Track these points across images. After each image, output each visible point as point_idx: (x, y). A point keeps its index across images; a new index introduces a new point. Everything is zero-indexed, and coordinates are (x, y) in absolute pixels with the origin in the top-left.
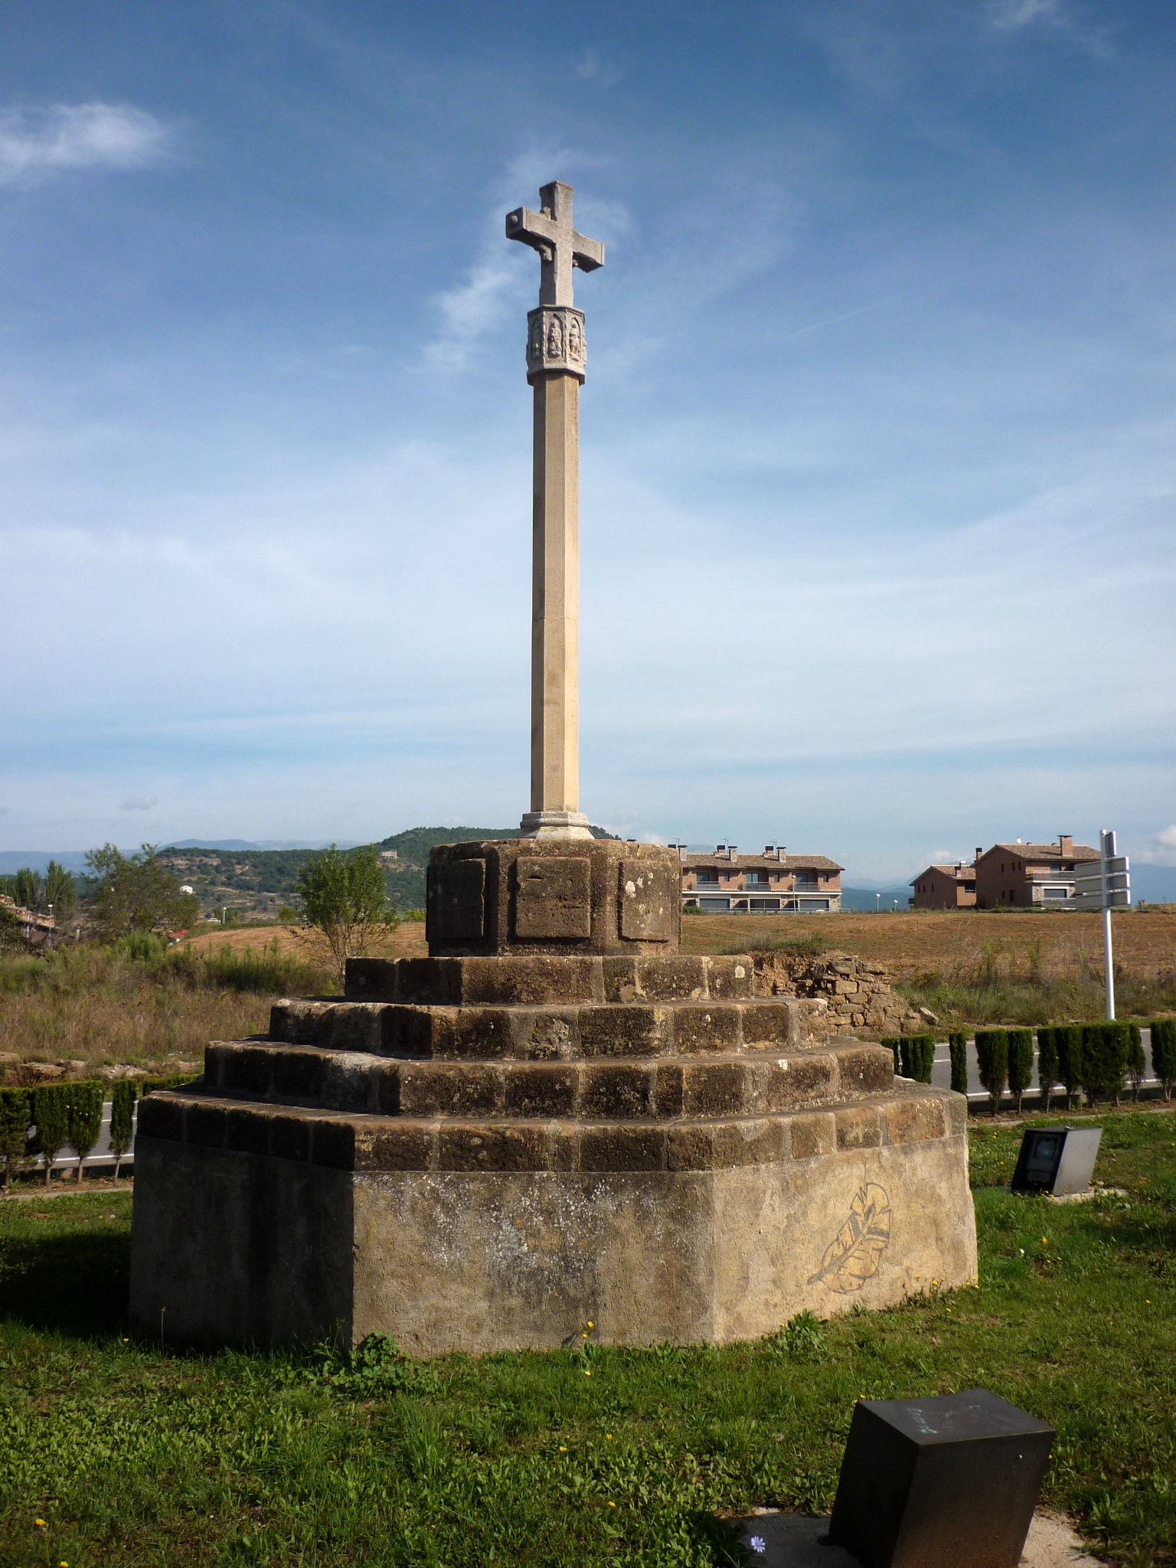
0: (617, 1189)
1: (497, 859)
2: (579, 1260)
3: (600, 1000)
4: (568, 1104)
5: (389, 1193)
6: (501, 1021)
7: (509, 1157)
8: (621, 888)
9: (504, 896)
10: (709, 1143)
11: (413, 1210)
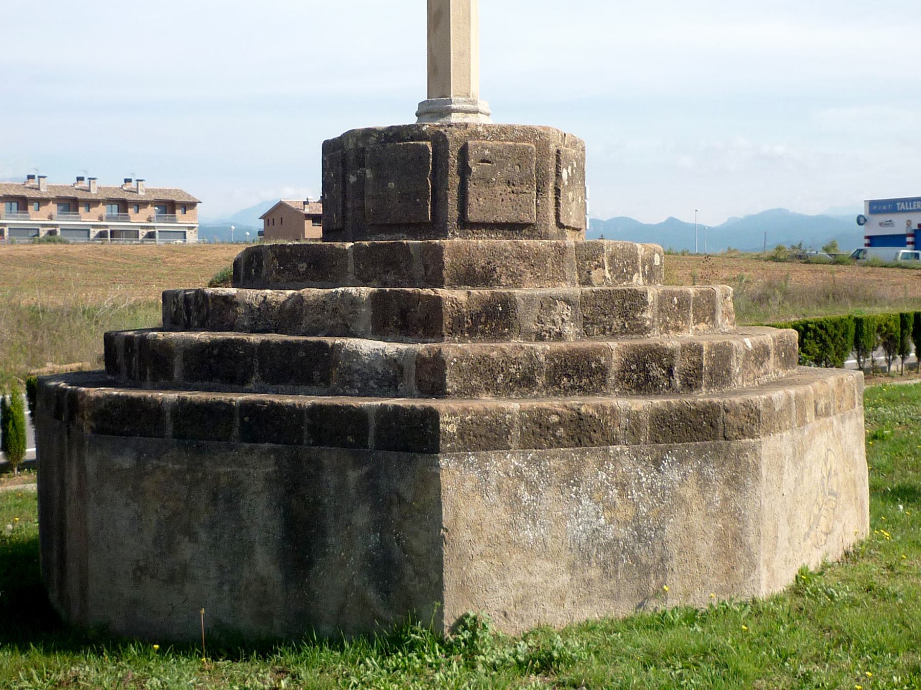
0: (682, 459)
1: (445, 141)
2: (651, 529)
3: (573, 284)
4: (603, 382)
5: (475, 474)
6: (507, 303)
7: (583, 432)
8: (558, 175)
9: (454, 180)
10: (758, 413)
11: (499, 490)
